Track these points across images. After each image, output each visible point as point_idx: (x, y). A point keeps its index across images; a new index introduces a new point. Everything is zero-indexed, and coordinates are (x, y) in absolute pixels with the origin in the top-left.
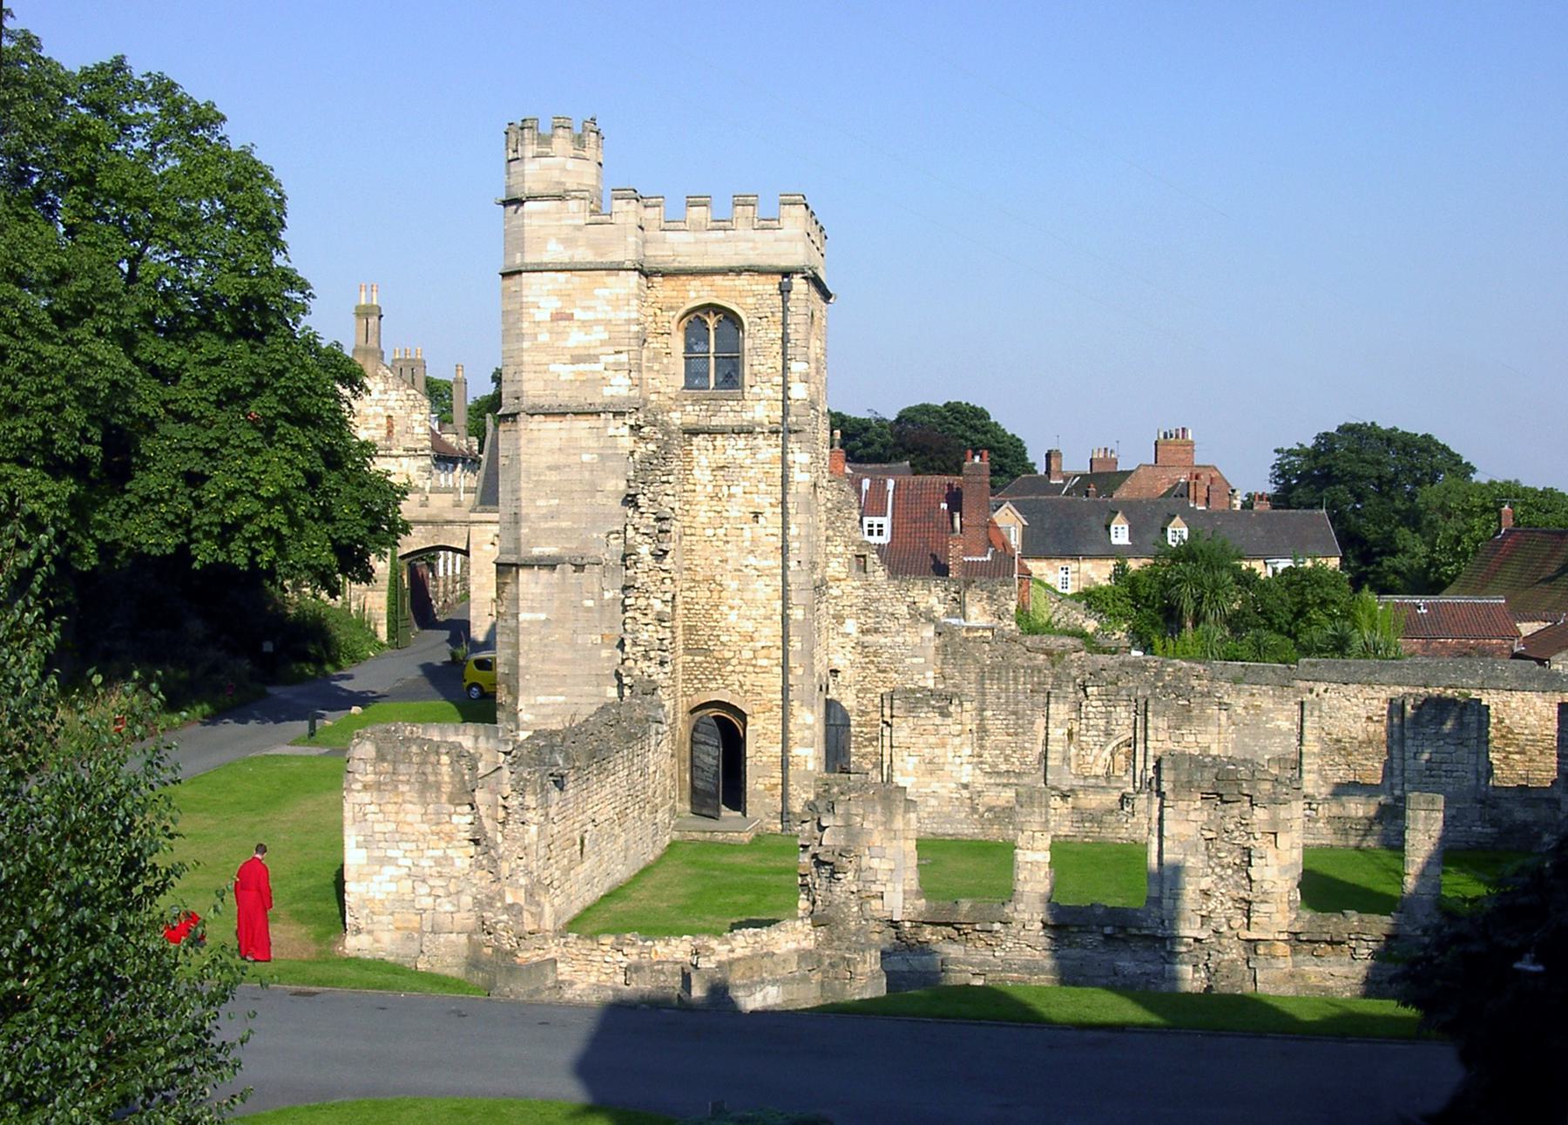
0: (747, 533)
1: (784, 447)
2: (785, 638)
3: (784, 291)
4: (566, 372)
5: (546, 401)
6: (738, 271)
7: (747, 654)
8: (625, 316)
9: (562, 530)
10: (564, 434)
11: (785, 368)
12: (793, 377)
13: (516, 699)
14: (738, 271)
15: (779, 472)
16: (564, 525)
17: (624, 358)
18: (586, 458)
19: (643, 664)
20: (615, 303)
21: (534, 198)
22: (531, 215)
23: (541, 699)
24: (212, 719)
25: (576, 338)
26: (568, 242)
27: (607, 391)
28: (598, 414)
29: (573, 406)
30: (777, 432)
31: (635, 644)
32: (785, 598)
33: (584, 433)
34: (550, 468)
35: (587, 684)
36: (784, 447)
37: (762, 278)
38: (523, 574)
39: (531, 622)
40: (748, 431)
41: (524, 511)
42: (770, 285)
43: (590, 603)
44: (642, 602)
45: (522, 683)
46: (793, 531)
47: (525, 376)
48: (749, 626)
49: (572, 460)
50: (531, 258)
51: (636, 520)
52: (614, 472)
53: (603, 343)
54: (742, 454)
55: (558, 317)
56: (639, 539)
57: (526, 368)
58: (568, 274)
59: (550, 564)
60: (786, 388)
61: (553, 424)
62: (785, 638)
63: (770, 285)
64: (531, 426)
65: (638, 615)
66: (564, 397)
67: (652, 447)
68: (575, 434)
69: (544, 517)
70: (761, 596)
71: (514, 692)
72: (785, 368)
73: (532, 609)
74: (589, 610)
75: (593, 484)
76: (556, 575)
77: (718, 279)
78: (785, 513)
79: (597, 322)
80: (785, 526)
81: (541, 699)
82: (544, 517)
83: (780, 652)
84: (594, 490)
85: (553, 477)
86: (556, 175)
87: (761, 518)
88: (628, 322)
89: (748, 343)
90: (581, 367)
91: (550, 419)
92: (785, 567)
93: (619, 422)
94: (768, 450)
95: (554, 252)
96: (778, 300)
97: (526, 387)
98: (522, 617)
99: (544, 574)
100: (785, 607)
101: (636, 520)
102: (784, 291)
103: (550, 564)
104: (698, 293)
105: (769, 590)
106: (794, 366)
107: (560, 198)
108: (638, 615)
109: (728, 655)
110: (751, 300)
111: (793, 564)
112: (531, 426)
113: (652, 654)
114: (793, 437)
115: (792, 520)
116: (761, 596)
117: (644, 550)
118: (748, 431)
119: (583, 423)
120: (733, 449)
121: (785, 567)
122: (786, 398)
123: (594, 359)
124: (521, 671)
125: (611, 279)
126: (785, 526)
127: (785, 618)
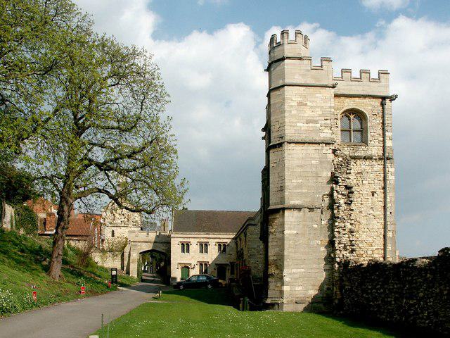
0: (370, 200)
1: (384, 165)
2: (385, 245)
3: (383, 105)
4: (304, 126)
5: (296, 139)
6: (365, 96)
7: (370, 252)
8: (329, 105)
9: (302, 193)
10: (305, 152)
11: (384, 134)
12: (387, 138)
13: (282, 271)
14: (365, 96)
15: (382, 175)
16: (304, 191)
17: (329, 122)
18: (314, 162)
19: (344, 252)
20: (325, 100)
21: (289, 58)
22: (287, 64)
23: (294, 271)
24: (414, 260)
25: (308, 113)
26: (303, 76)
27: (322, 135)
28: (319, 143)
29: (308, 141)
30: (382, 159)
31: (340, 243)
32: (385, 228)
33: (313, 152)
34: (298, 166)
35: (314, 263)
36: (384, 165)
37: (374, 100)
38: (287, 213)
39: (290, 234)
40: (369, 158)
41: (286, 185)
42: (378, 102)
43: (315, 226)
44: (342, 225)
45: (285, 263)
46: (388, 200)
47: (286, 127)
48: (370, 240)
49: (307, 163)
50: (287, 81)
51: (338, 188)
52: (326, 168)
53: (320, 116)
54: (368, 168)
55: (300, 104)
56: (340, 196)
57: (286, 124)
58: (305, 88)
59: (299, 209)
60: (384, 142)
61: (299, 147)
62: (385, 245)
63: (378, 102)
64: (290, 148)
65: (341, 230)
66: (303, 137)
67: (341, 159)
68: (309, 152)
69: (296, 188)
70: (375, 227)
71: (280, 267)
72: (384, 134)
73: (290, 229)
74: (315, 229)
75: (317, 174)
76: (301, 213)
77: (357, 99)
78: (385, 193)
79: (318, 107)
80: (385, 197)
81: (294, 271)
82: (296, 188)
83: (382, 252)
84: (317, 176)
85: (299, 170)
86: (298, 51)
87: (375, 195)
88: (330, 107)
89: (369, 124)
90: (311, 125)
91: (297, 145)
92: (385, 215)
93: (328, 147)
94: (378, 166)
95: (297, 79)
96: (380, 108)
97: (286, 132)
98: (285, 232)
99: (296, 213)
100: (385, 232)
101: (338, 188)
102: (383, 105)
103: (299, 209)
104: (349, 104)
105: (379, 224)
106: (387, 134)
107: (301, 59)
108: (341, 230)
109: (362, 252)
110: (370, 108)
111: (388, 213)
112: (290, 148)
113: (348, 247)
114: (388, 161)
115: (388, 195)
116: (375, 227)
117: (342, 201)
118: (369, 158)
119: (311, 147)
120: (362, 165)
121: (385, 215)
122: (384, 147)
123: (315, 122)
124: (285, 258)
125: (323, 90)
126: (385, 197)
127: (385, 237)
